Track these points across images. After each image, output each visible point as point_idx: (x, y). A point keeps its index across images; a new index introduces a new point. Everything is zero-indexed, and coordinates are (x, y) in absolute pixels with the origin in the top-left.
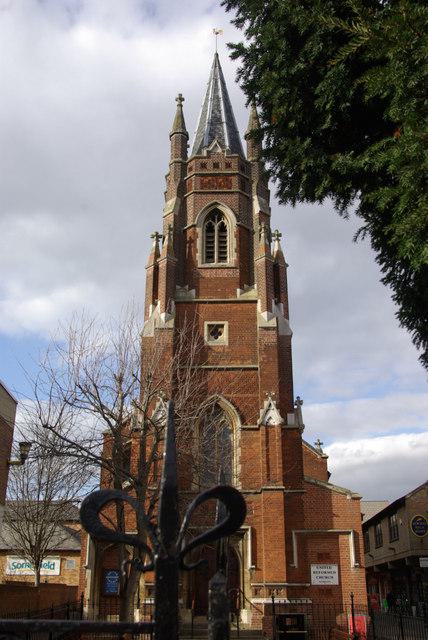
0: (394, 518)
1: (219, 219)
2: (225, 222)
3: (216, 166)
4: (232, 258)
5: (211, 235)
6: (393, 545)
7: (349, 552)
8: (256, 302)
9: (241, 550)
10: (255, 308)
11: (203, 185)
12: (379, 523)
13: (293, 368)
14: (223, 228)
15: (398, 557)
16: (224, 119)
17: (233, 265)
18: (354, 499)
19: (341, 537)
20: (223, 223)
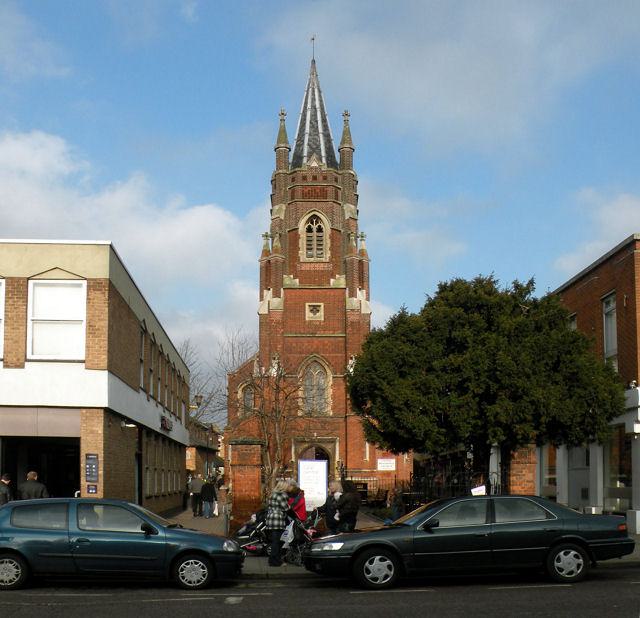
2: (322, 226)
4: (328, 255)
10: (344, 293)
14: (320, 230)
17: (328, 260)
20: (320, 226)
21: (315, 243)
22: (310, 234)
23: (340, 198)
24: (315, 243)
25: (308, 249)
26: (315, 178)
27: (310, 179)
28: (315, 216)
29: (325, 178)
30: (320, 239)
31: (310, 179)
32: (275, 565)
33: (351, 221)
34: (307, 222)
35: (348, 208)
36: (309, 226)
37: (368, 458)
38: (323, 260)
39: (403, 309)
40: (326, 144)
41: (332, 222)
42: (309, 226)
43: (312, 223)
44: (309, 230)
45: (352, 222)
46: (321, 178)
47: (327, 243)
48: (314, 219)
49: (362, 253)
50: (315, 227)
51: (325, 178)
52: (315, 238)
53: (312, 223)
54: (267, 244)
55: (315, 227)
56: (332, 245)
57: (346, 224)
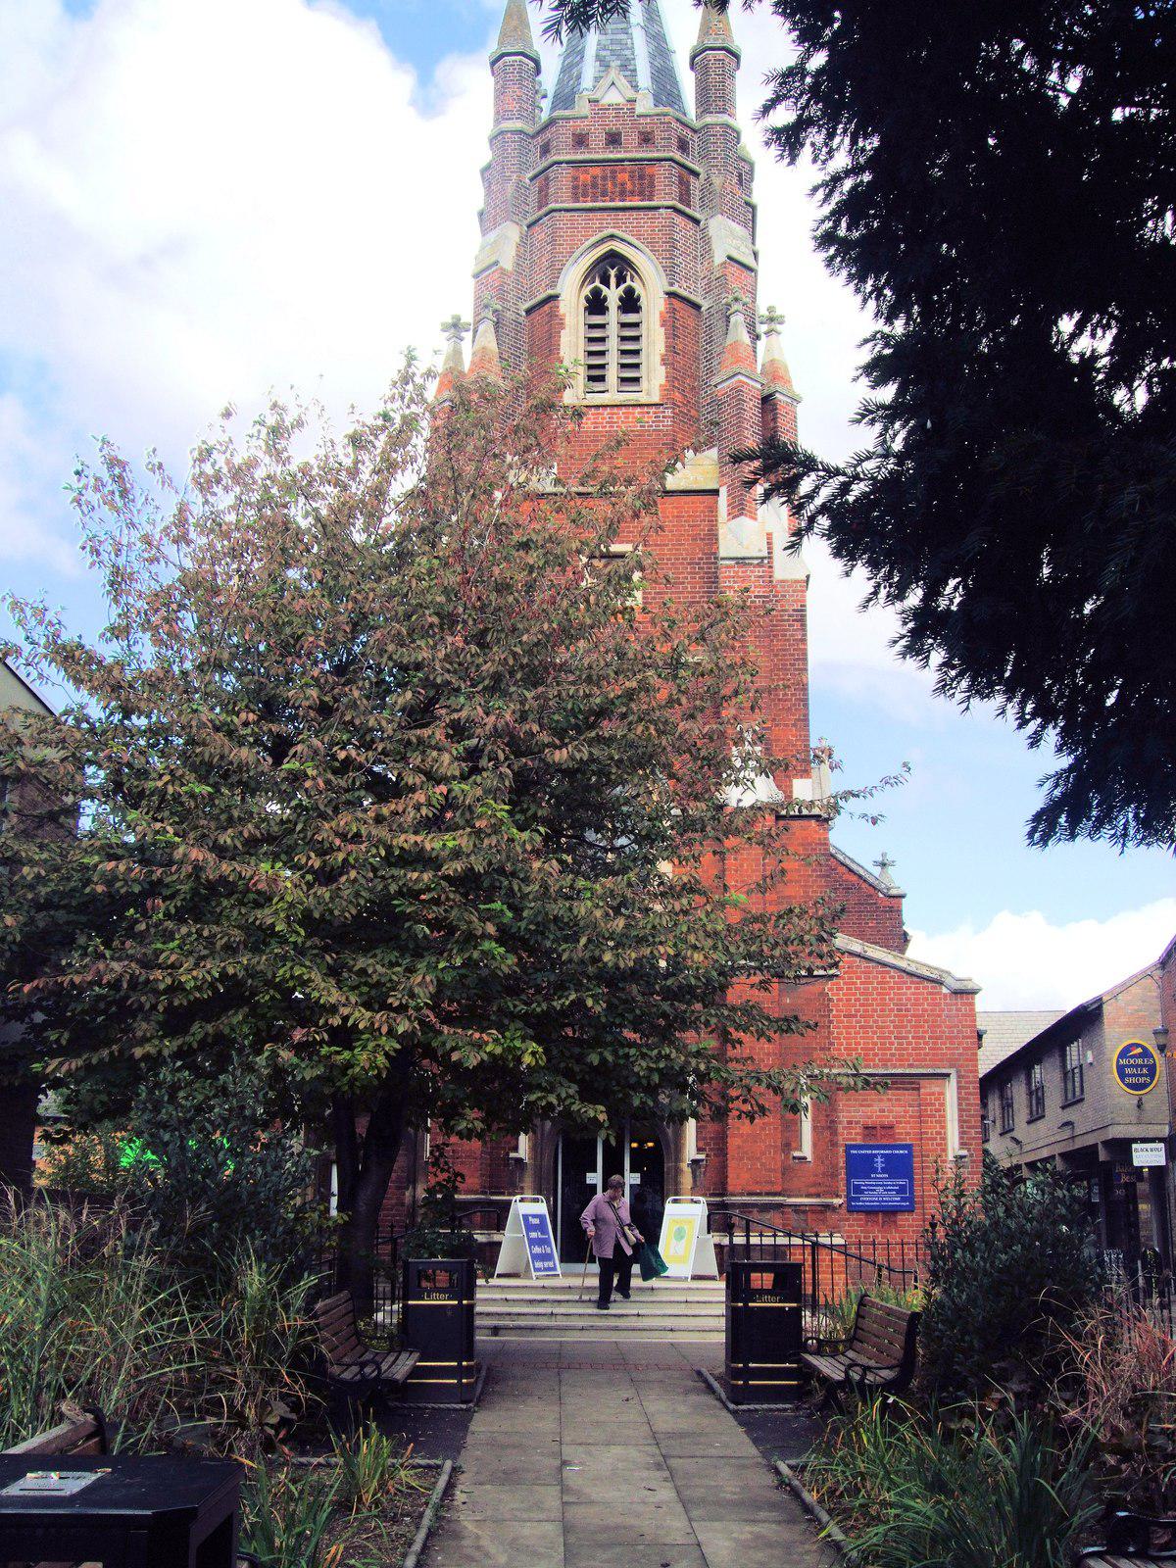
0: (1073, 1050)
1: (621, 280)
2: (637, 286)
3: (580, 140)
4: (654, 379)
5: (879, 1163)
6: (1071, 1115)
7: (942, 1122)
8: (716, 492)
9: (809, 1290)
10: (713, 510)
11: (577, 192)
12: (1039, 1062)
13: (1003, 1058)
14: (630, 303)
15: (1079, 1144)
16: (417, 1547)
17: (656, 399)
18: (957, 993)
19: (929, 1087)
20: (630, 291)
21: (613, 360)
22: (597, 319)
23: (695, 199)
24: (613, 360)
25: (591, 378)
26: (614, 139)
27: (631, 139)
28: (613, 258)
29: (646, 139)
30: (631, 336)
31: (597, 139)
32: (652, 185)
33: (734, 269)
34: (588, 276)
35: (724, 236)
36: (596, 293)
37: (807, 1150)
38: (643, 398)
39: (1045, 826)
40: (652, 56)
41: (671, 271)
42: (596, 293)
43: (606, 281)
44: (596, 305)
45: (735, 279)
46: (635, 138)
47: (654, 341)
48: (616, 264)
49: (774, 372)
50: (613, 295)
51: (646, 139)
52: (613, 331)
53: (606, 281)
54: (457, 354)
55: (613, 295)
56: (671, 349)
57: (717, 283)
